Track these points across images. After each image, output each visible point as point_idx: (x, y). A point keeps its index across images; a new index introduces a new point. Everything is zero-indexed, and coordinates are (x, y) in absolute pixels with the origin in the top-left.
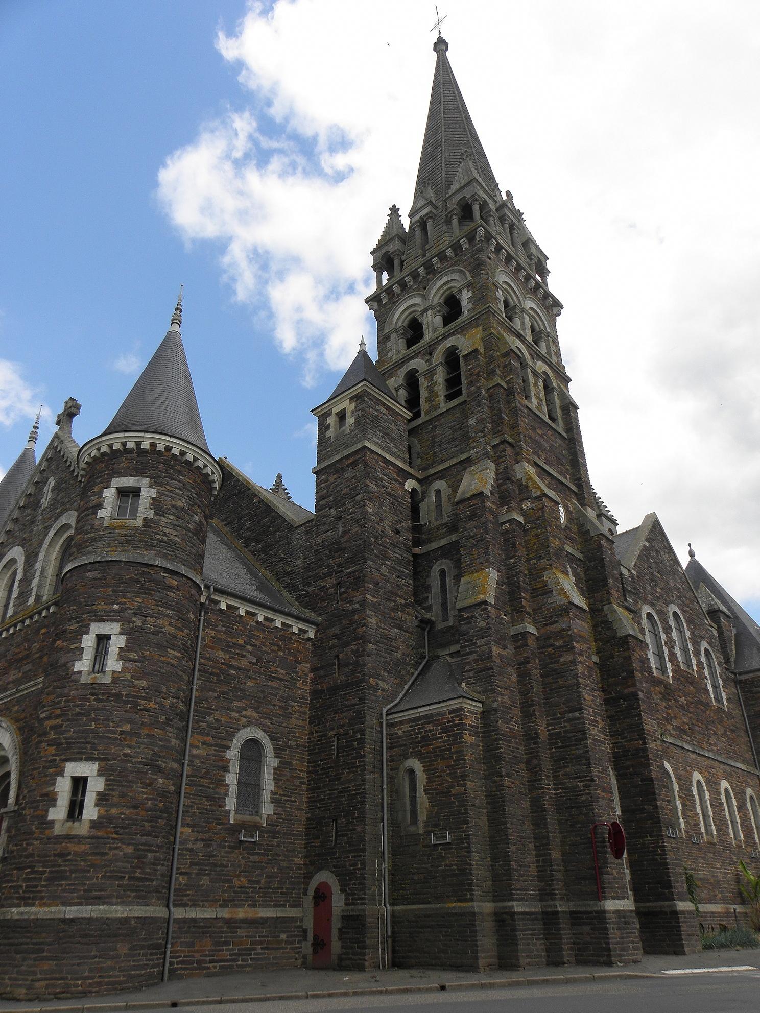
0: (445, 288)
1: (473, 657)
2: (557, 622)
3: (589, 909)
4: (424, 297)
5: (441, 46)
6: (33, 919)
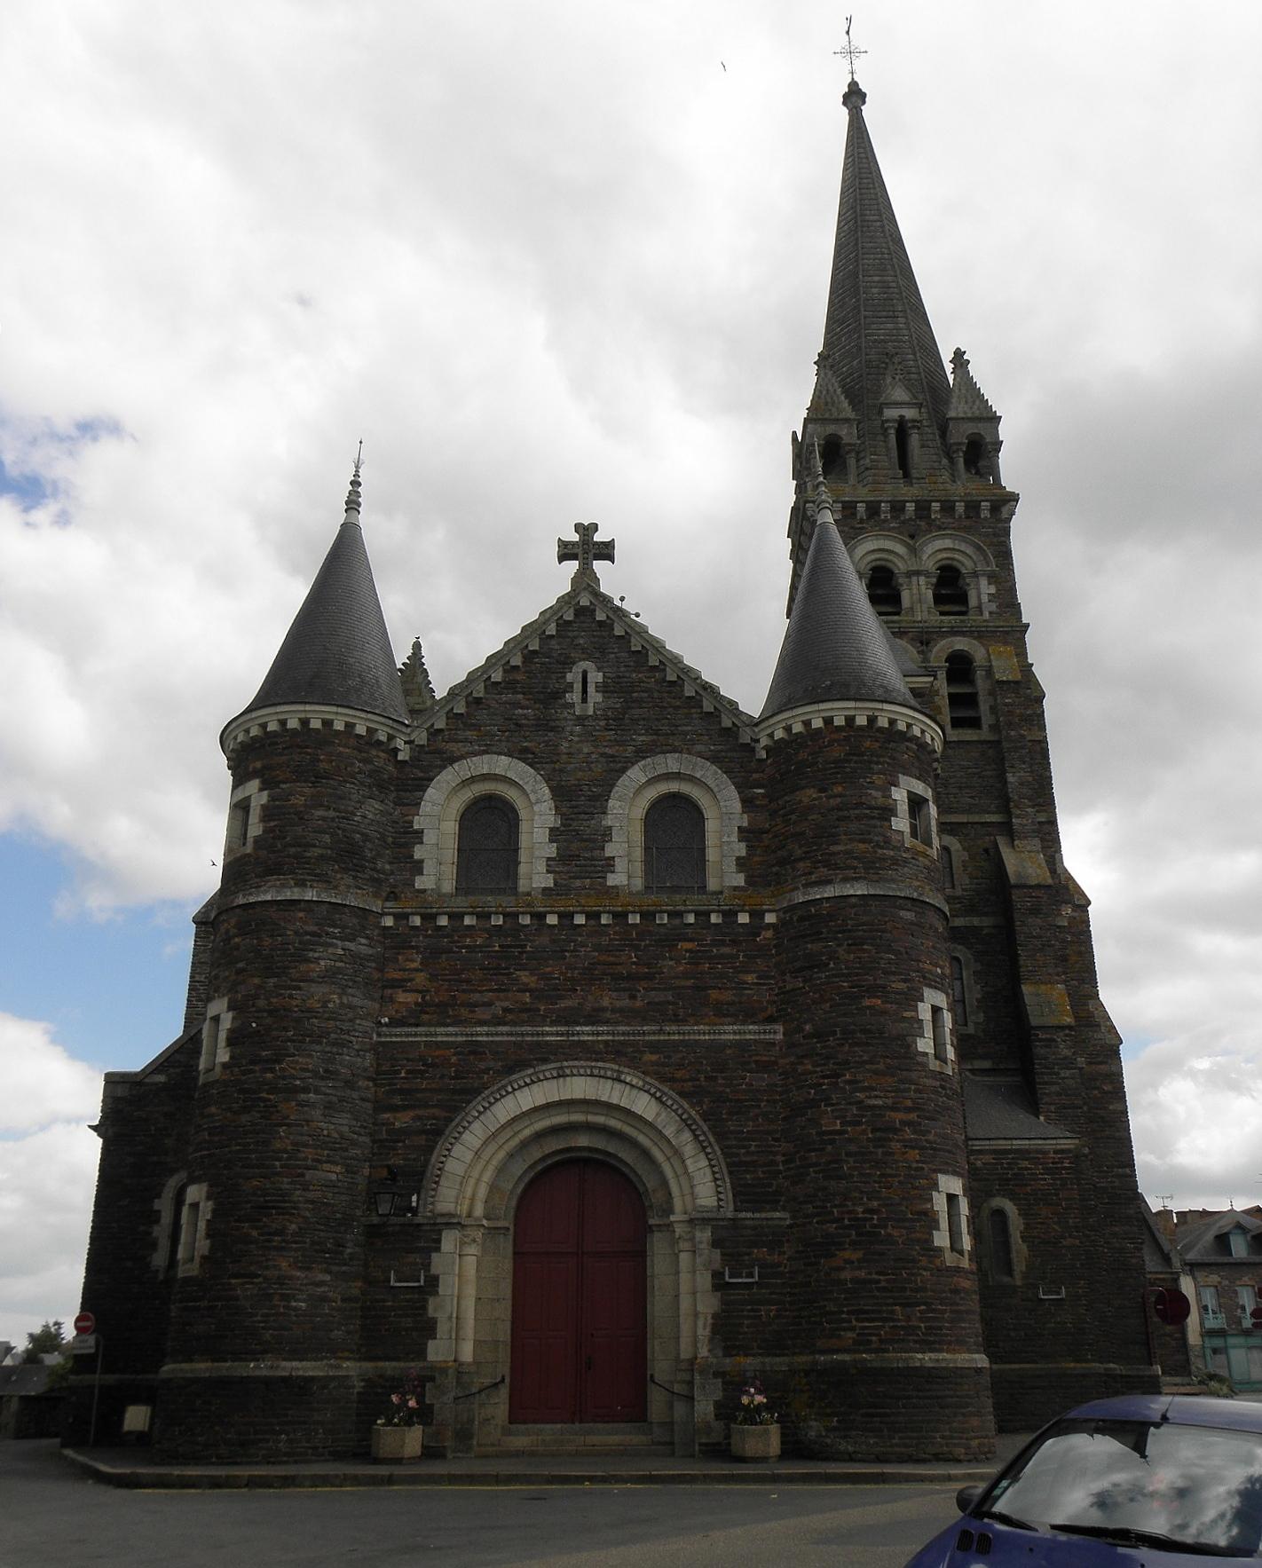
0: (945, 555)
1: (1054, 1088)
2: (1106, 1063)
3: (1141, 1373)
4: (914, 551)
5: (854, 97)
6: (953, 1367)
